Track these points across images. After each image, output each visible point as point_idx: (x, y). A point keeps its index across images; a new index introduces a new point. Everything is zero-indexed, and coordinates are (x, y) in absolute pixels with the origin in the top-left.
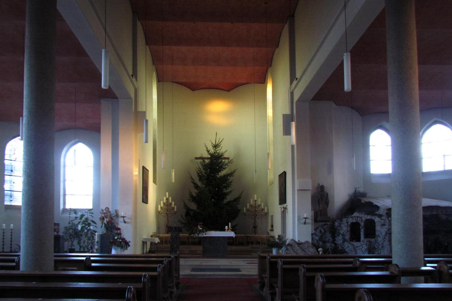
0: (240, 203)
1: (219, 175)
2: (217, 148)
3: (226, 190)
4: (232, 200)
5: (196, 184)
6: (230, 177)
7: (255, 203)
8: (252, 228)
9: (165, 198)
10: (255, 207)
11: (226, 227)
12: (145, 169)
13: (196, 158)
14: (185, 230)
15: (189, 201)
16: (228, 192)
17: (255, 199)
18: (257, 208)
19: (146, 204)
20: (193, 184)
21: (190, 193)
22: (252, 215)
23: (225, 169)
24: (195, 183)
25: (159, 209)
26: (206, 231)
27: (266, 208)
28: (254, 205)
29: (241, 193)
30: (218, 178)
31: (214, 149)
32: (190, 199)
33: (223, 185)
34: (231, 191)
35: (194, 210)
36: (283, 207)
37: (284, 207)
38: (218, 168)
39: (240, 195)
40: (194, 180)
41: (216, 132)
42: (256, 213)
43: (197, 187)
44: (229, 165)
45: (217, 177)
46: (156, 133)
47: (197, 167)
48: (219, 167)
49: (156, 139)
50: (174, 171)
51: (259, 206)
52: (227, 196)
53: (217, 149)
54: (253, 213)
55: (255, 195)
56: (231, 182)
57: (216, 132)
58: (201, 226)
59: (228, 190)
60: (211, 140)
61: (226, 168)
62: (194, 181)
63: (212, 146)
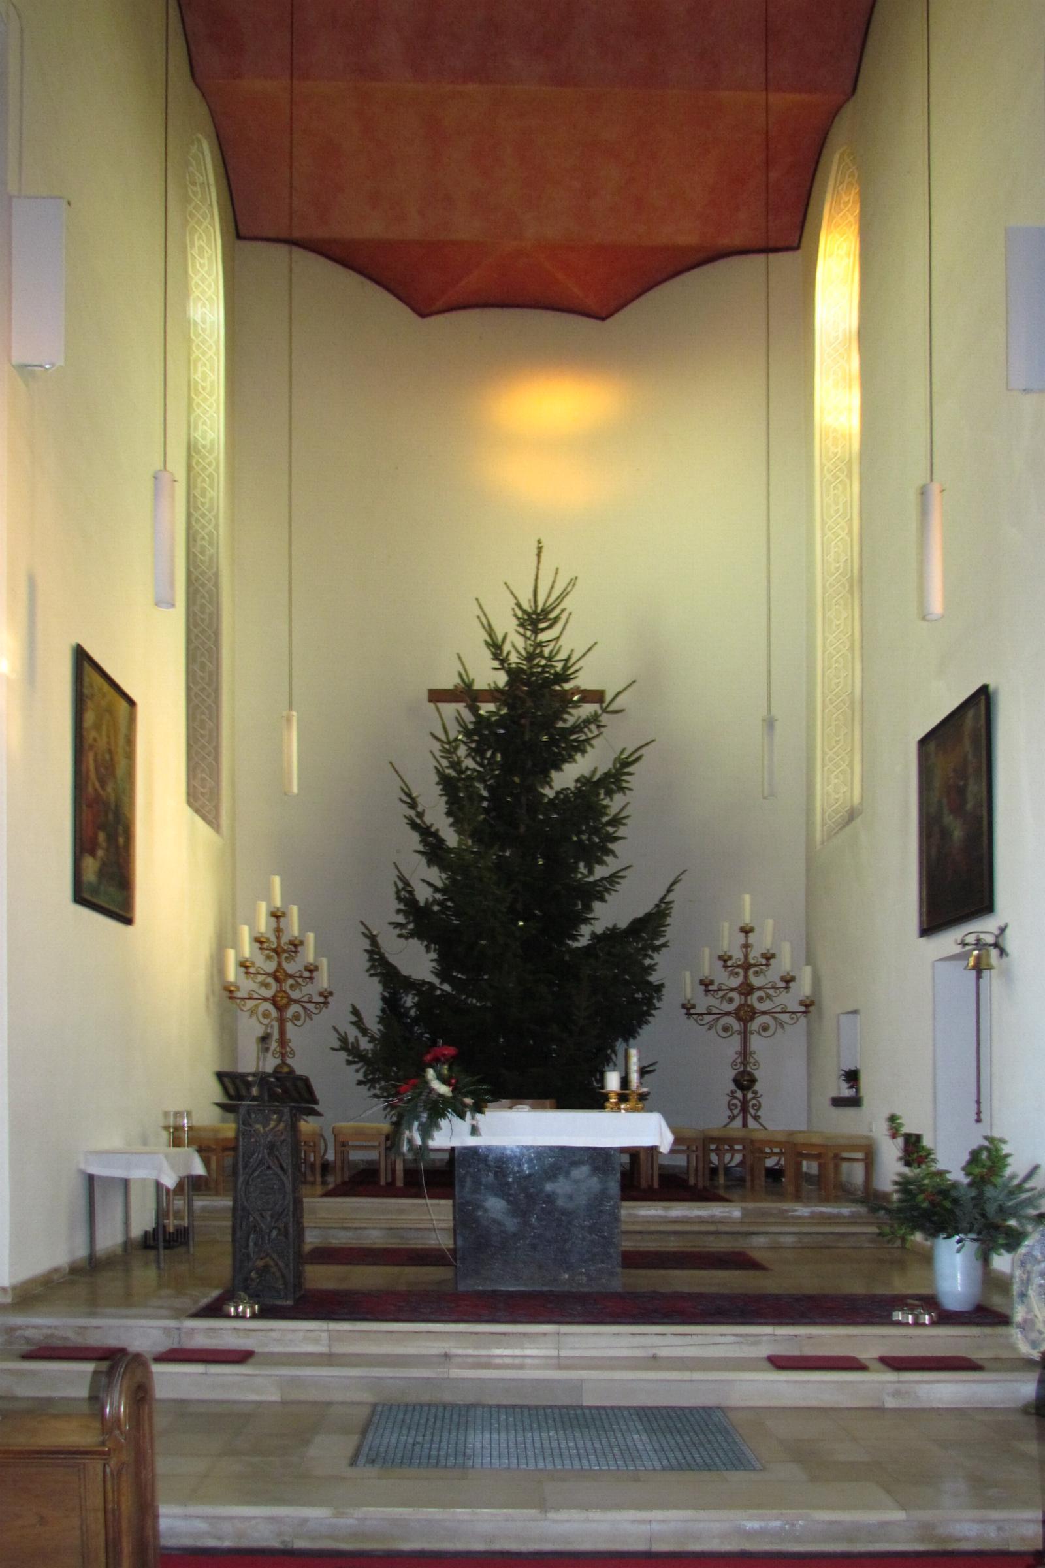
0: (665, 945)
1: (551, 787)
2: (543, 630)
3: (591, 872)
4: (623, 924)
5: (435, 835)
6: (609, 793)
7: (746, 946)
8: (732, 1087)
9: (263, 908)
10: (747, 966)
11: (613, 1081)
12: (87, 668)
13: (437, 696)
14: (375, 1096)
15: (397, 931)
16: (603, 879)
17: (747, 919)
18: (756, 973)
19: (1000, 1330)
20: (415, 837)
21: (401, 885)
22: (728, 1014)
23: (583, 752)
24: (428, 828)
25: (232, 973)
26: (478, 1108)
27: (808, 970)
28: (742, 957)
29: (669, 891)
30: (546, 800)
31: (524, 636)
32: (401, 919)
33: (575, 838)
34: (613, 879)
35: (424, 983)
36: (971, 939)
37: (978, 940)
38: (545, 739)
39: (662, 900)
40: (420, 809)
41: (539, 542)
42: (753, 1000)
43: (434, 850)
44: (604, 726)
45: (544, 795)
46: (217, 527)
47: (437, 734)
48: (551, 737)
49: (218, 568)
50: (298, 721)
51: (769, 957)
52: (597, 905)
53: (543, 637)
54: (731, 1000)
55: (747, 898)
56: (616, 821)
57: (539, 542)
58: (445, 1070)
59: (600, 872)
60: (509, 584)
61: (588, 740)
62: (420, 815)
63: (515, 615)
